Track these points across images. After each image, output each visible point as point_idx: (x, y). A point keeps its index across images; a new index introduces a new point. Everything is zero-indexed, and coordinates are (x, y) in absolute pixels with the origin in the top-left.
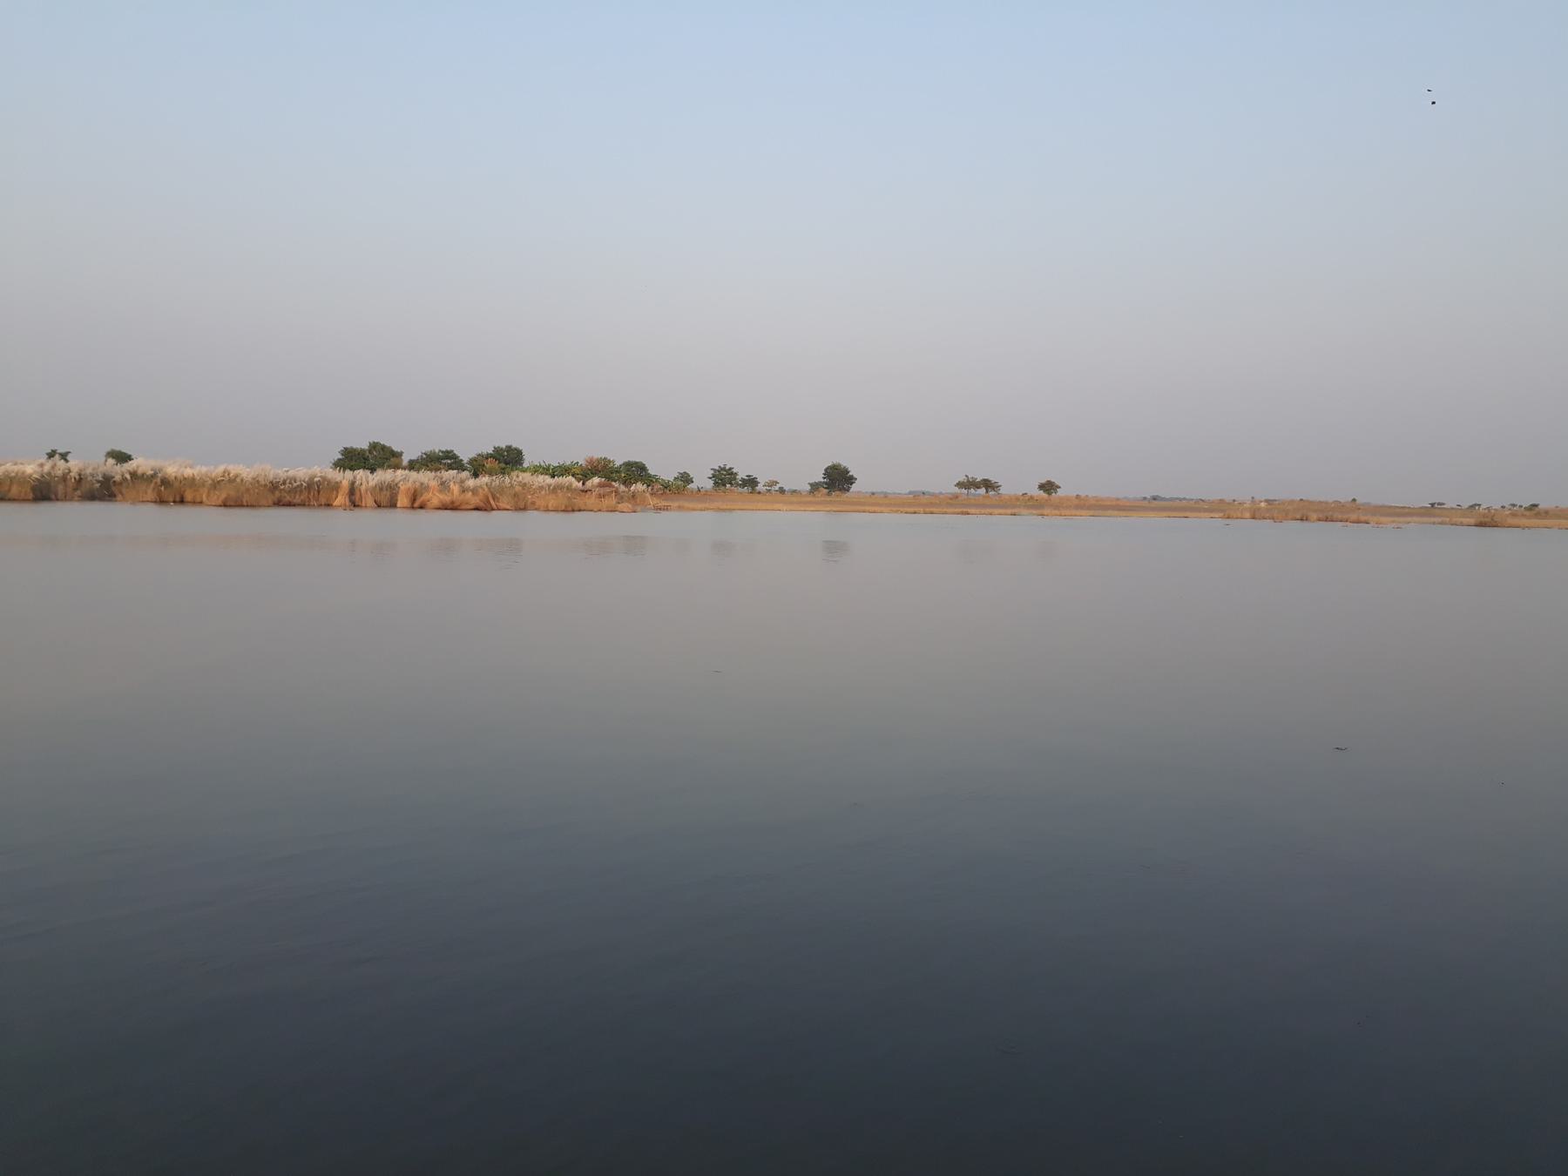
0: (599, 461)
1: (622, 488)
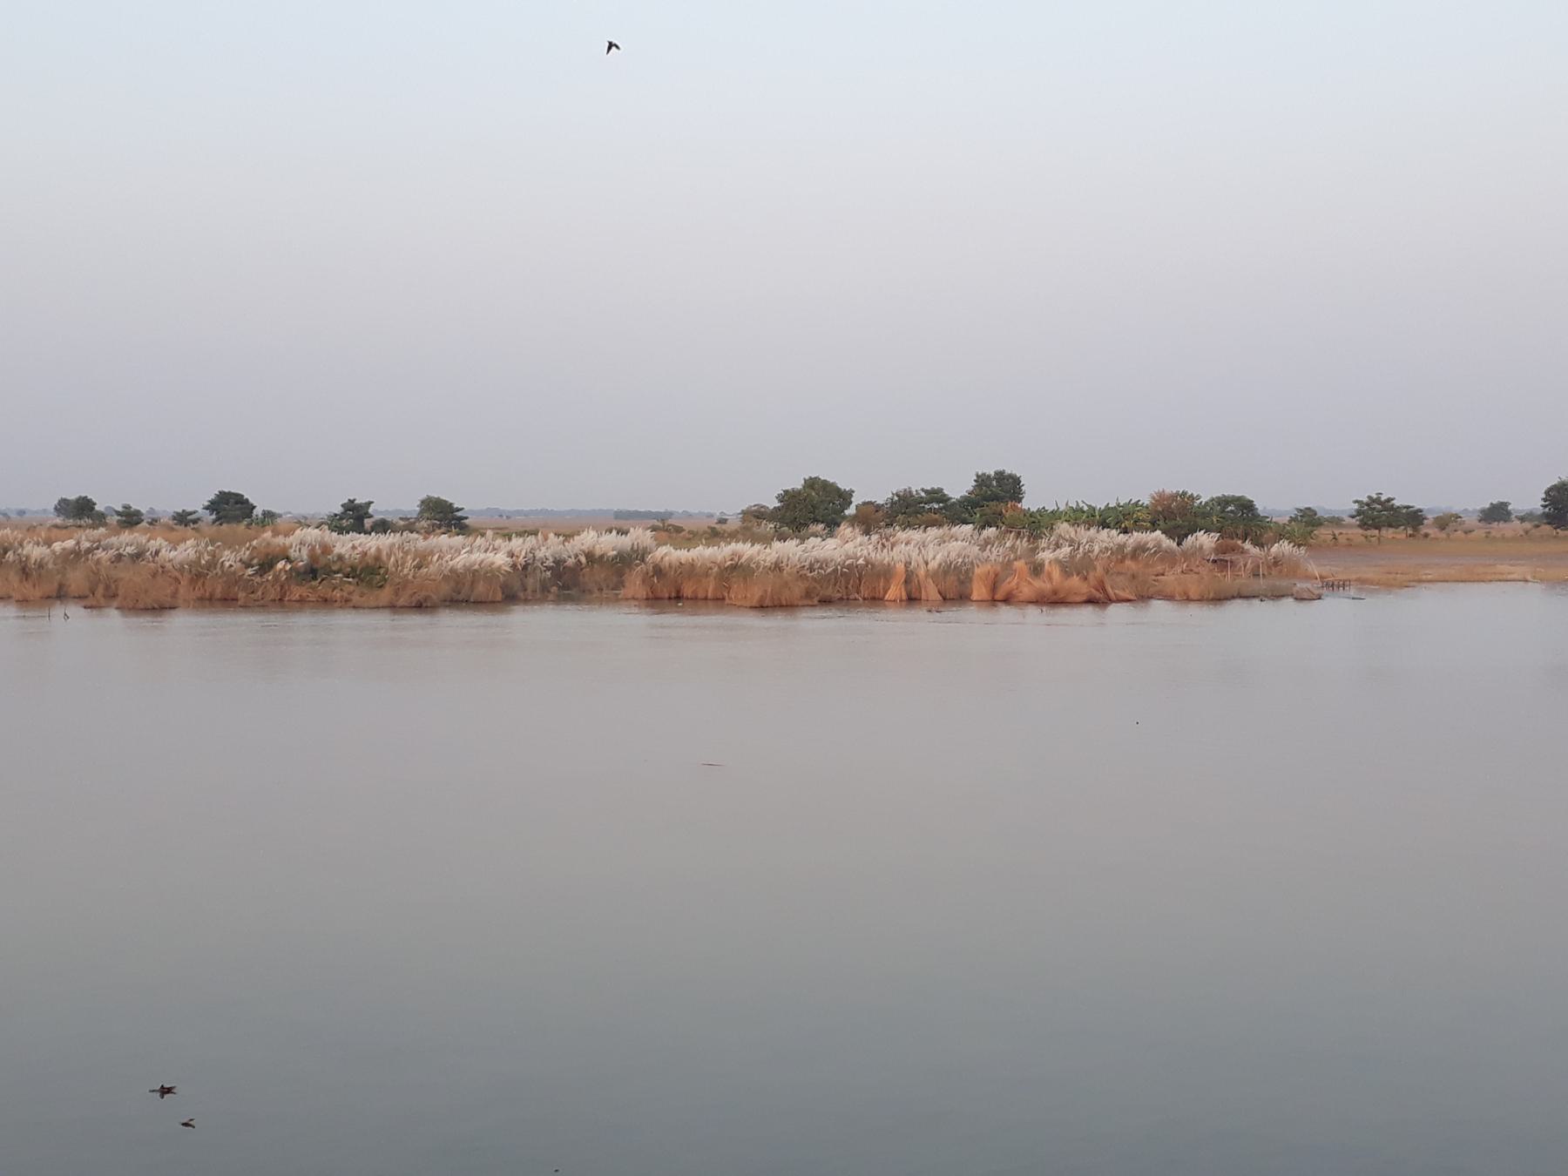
0: (1174, 497)
1: (1255, 551)
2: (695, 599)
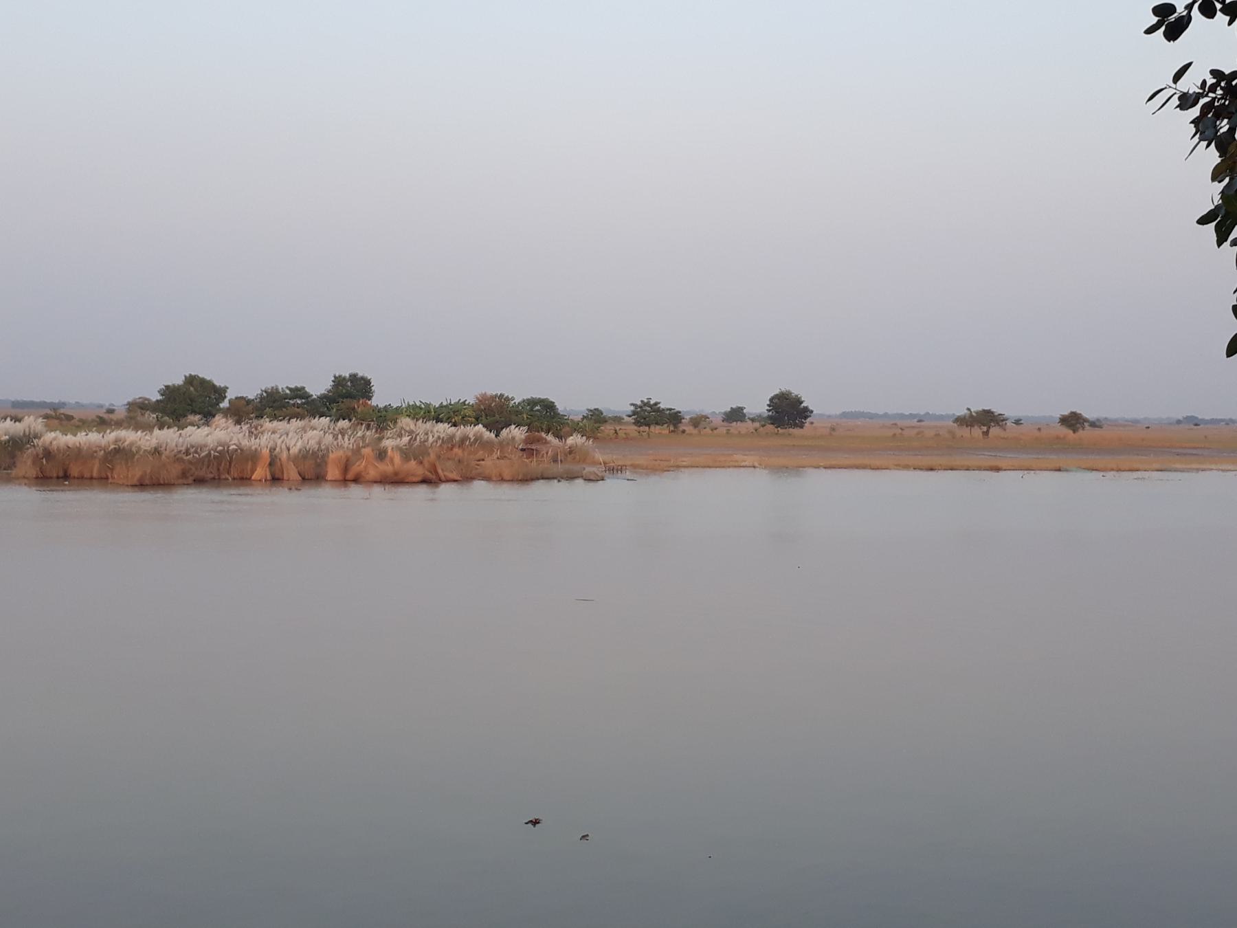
0: (493, 398)
2: (81, 478)
